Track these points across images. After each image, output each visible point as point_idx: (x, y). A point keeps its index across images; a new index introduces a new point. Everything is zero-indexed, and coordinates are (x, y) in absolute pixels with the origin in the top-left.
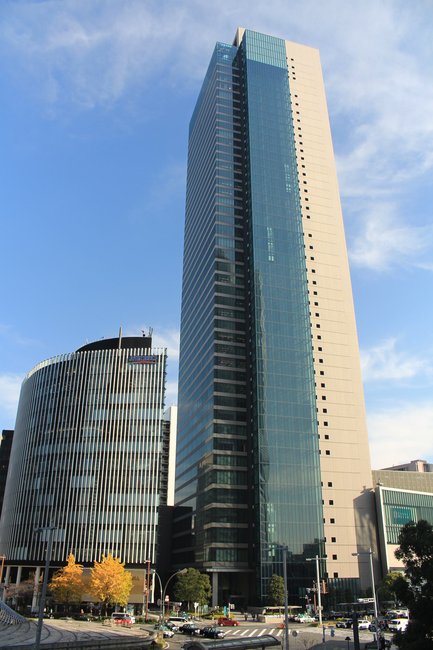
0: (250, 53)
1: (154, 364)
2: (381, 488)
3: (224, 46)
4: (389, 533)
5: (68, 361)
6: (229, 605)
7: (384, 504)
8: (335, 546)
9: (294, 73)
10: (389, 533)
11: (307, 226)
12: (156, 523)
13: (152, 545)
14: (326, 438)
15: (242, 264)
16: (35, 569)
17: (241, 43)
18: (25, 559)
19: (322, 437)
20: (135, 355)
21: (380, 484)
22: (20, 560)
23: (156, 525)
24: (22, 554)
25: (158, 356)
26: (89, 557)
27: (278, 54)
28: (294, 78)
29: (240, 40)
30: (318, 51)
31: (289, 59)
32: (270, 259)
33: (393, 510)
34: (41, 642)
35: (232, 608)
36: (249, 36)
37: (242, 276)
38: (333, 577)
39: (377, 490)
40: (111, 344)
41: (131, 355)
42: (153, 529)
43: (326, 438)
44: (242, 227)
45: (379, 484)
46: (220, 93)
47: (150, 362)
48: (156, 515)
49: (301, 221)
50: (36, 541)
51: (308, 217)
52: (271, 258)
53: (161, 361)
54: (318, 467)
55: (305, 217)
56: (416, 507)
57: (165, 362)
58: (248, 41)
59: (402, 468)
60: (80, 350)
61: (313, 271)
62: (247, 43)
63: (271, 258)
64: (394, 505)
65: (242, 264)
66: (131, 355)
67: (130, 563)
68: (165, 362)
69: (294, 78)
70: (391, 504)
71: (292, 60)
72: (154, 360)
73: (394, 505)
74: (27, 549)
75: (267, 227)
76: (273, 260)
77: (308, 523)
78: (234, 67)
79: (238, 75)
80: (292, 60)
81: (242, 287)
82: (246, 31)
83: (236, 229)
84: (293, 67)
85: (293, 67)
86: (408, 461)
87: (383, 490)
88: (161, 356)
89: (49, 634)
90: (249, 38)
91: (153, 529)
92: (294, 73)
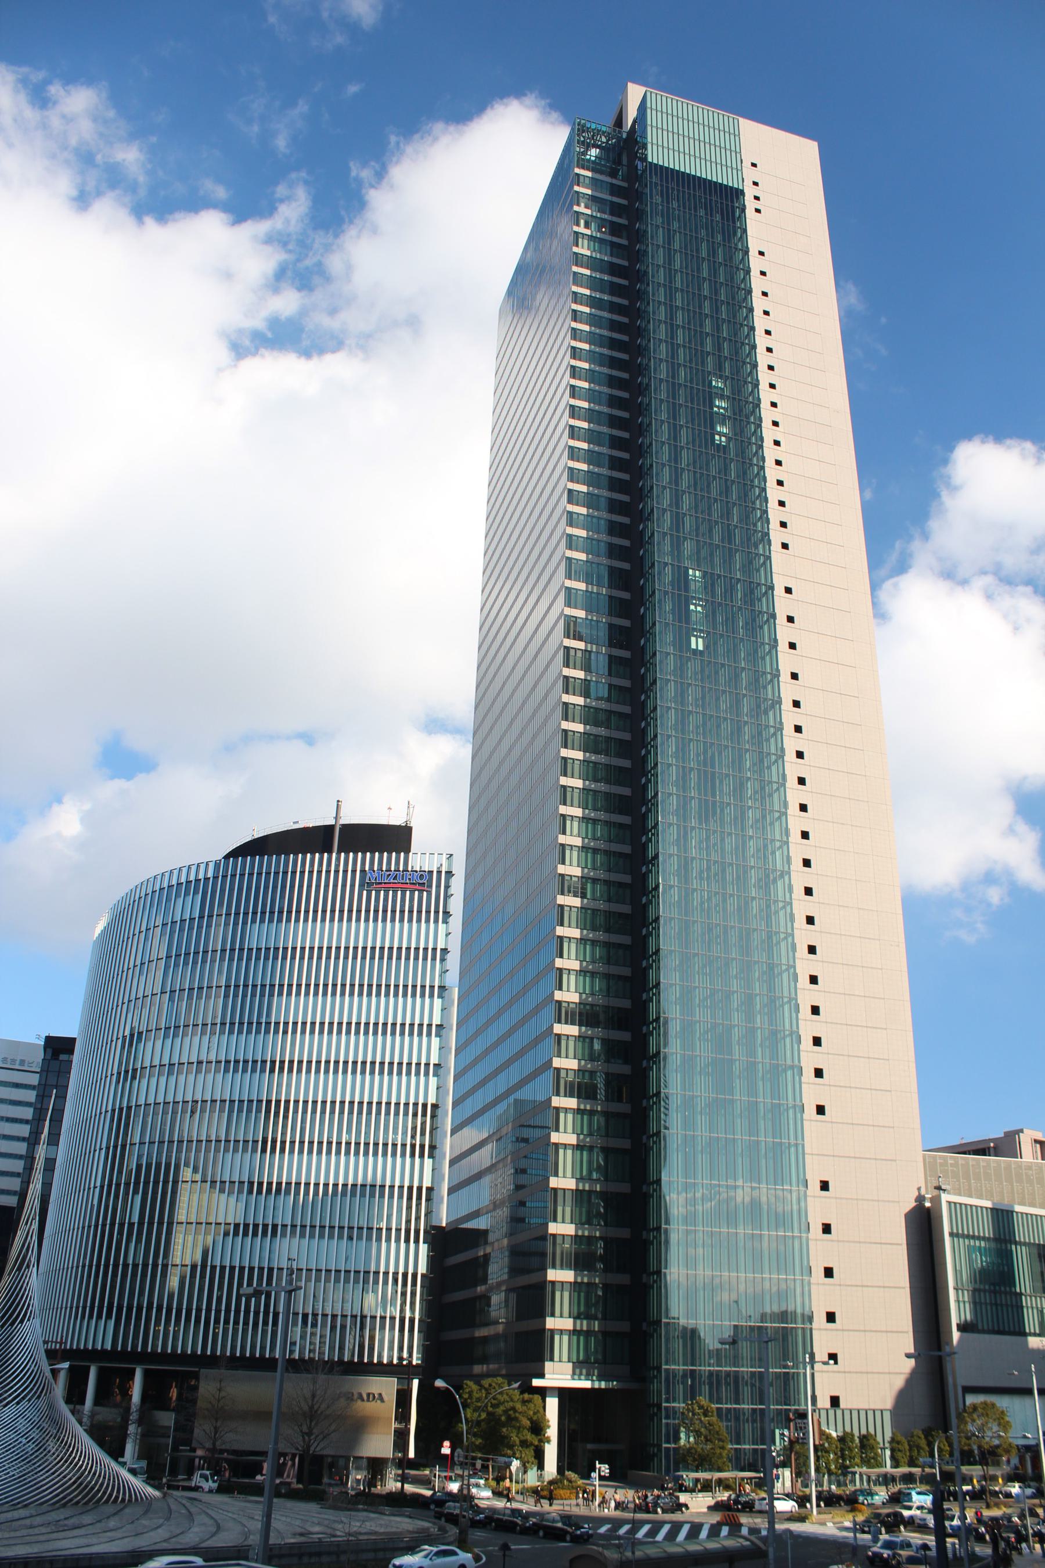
0: (655, 147)
1: (421, 892)
2: (945, 1197)
3: (593, 126)
4: (962, 1305)
5: (207, 879)
6: (598, 1466)
7: (951, 1234)
8: (834, 1333)
9: (757, 198)
10: (962, 1305)
11: (782, 568)
12: (422, 1269)
13: (412, 1321)
14: (816, 1076)
15: (626, 654)
16: (132, 1373)
17: (635, 122)
18: (108, 1346)
19: (809, 1074)
20: (376, 869)
21: (943, 1187)
22: (94, 1350)
23: (423, 1275)
24: (102, 1335)
25: (431, 872)
26: (332, 1348)
27: (718, 149)
28: (758, 211)
29: (631, 114)
30: (815, 145)
31: (747, 164)
32: (693, 646)
33: (970, 1249)
34: (271, 1542)
35: (602, 1474)
36: (654, 107)
37: (626, 683)
38: (828, 1405)
39: (936, 1200)
40: (316, 839)
41: (367, 868)
42: (414, 1284)
43: (816, 1076)
44: (626, 566)
45: (939, 1188)
46: (580, 240)
47: (413, 887)
48: (423, 1248)
49: (769, 558)
50: (175, 1306)
51: (785, 546)
52: (697, 643)
53: (438, 886)
54: (799, 1146)
55: (776, 546)
56: (1025, 1244)
57: (447, 887)
58: (651, 118)
59: (981, 1150)
60: (235, 854)
61: (794, 676)
62: (649, 122)
63: (697, 643)
64: (973, 1237)
65: (626, 654)
66: (367, 868)
67: (371, 1362)
68: (447, 887)
69: (758, 211)
70: (968, 1237)
71: (754, 165)
72: (422, 882)
73: (973, 1237)
74: (112, 1323)
75: (687, 569)
76: (701, 648)
77: (708, 1273)
78: (616, 178)
79: (624, 199)
80: (754, 165)
81: (626, 709)
82: (648, 94)
83: (612, 570)
84: (755, 184)
85: (755, 184)
86: (995, 1132)
87: (949, 1203)
88: (439, 872)
89: (219, 1528)
90: (654, 112)
91: (414, 1284)
92: (757, 198)
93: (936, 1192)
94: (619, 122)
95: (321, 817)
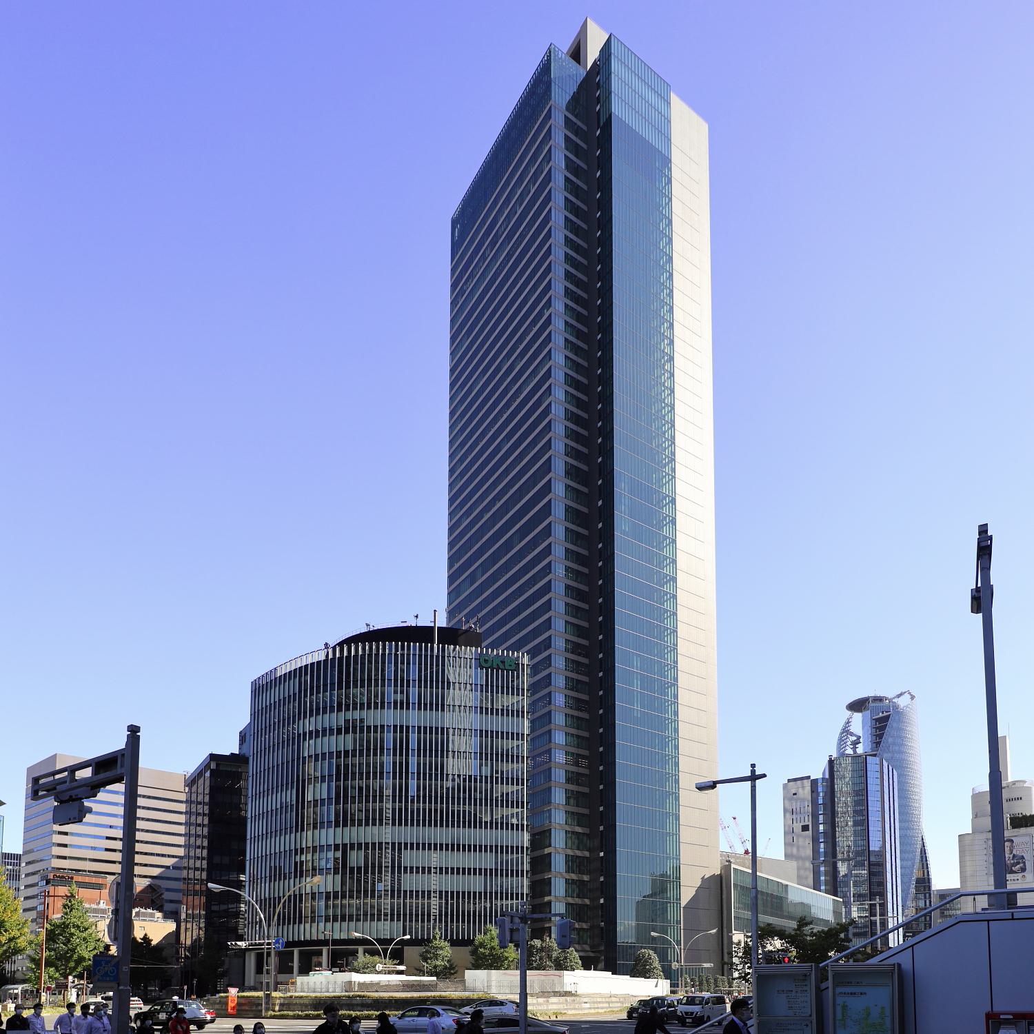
45: (729, 861)
93: (727, 863)
94: (577, 53)
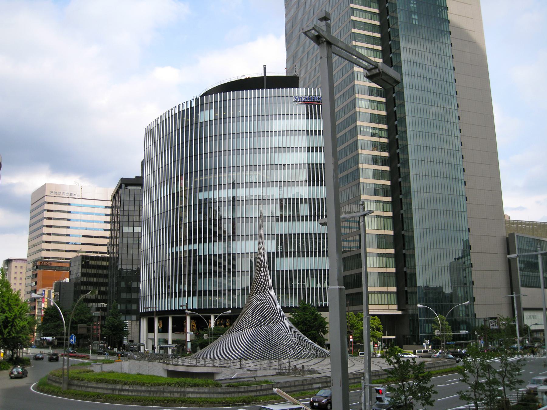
95: (257, 73)
